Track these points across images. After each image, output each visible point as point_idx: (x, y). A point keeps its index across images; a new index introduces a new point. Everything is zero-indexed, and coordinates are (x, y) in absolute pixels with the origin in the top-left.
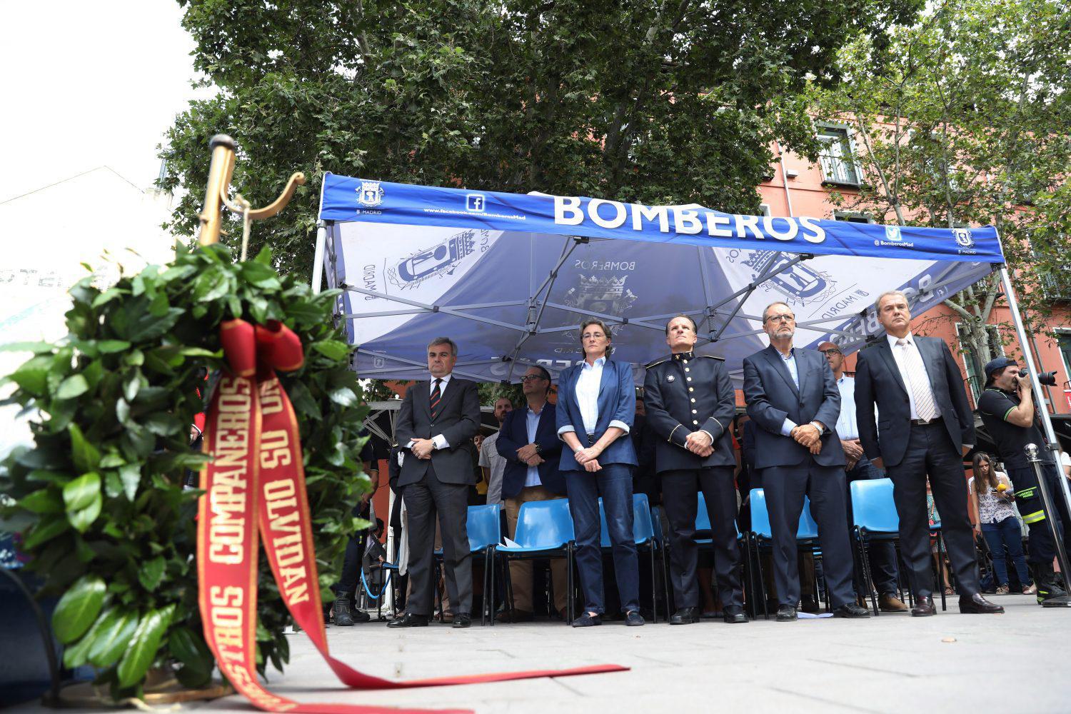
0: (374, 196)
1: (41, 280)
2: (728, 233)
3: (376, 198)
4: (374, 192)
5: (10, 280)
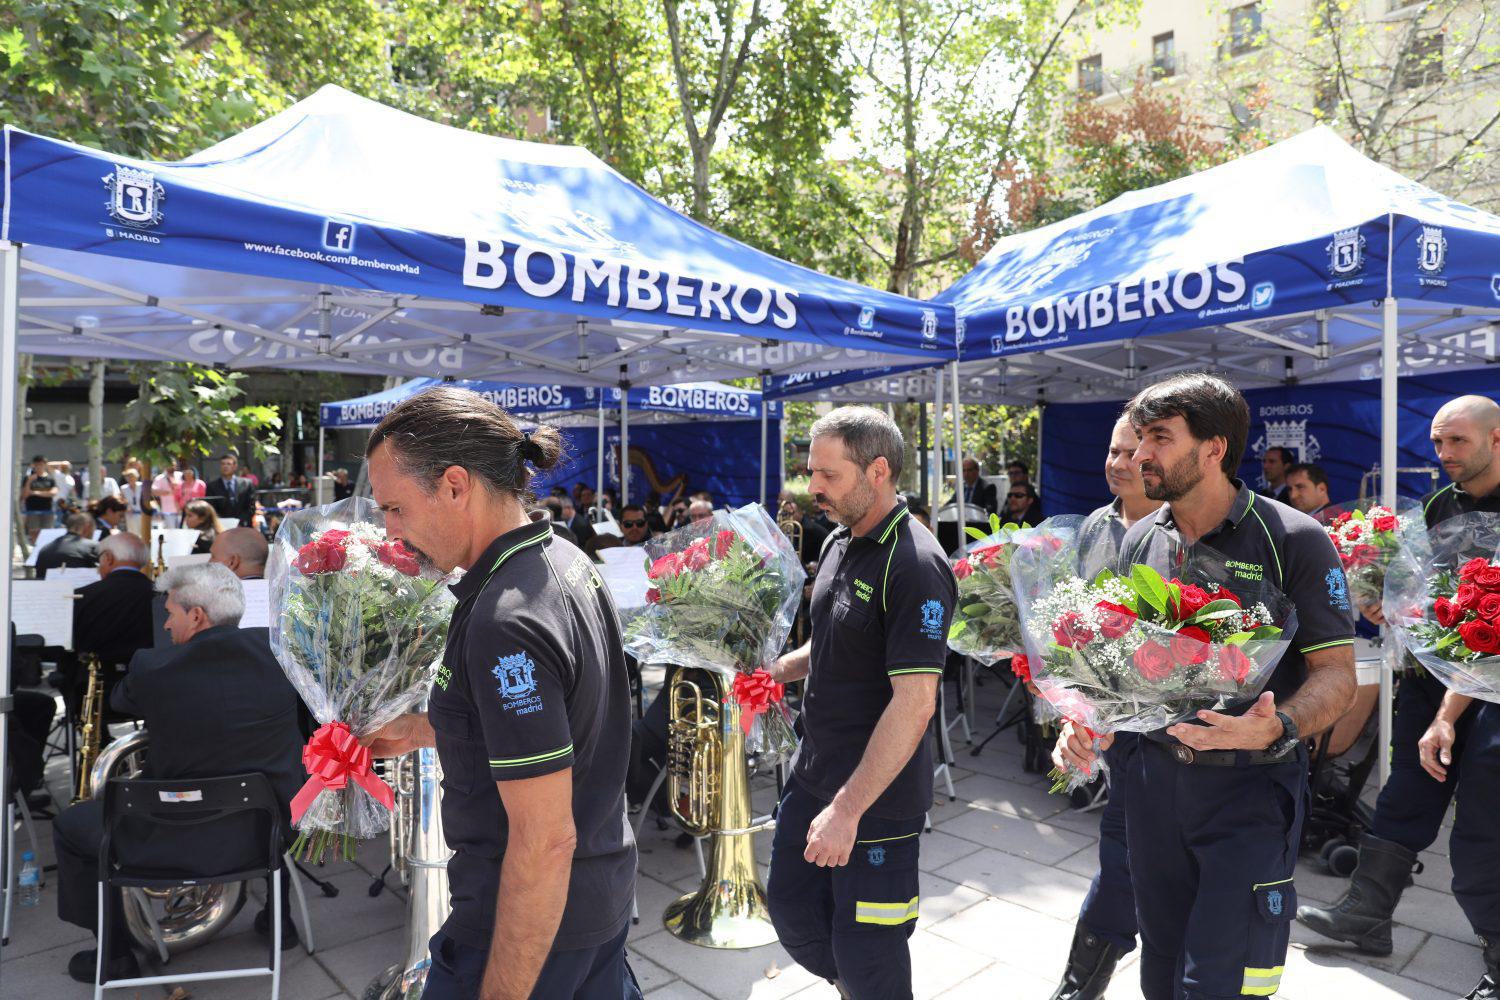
2: (690, 311)
4: (144, 191)
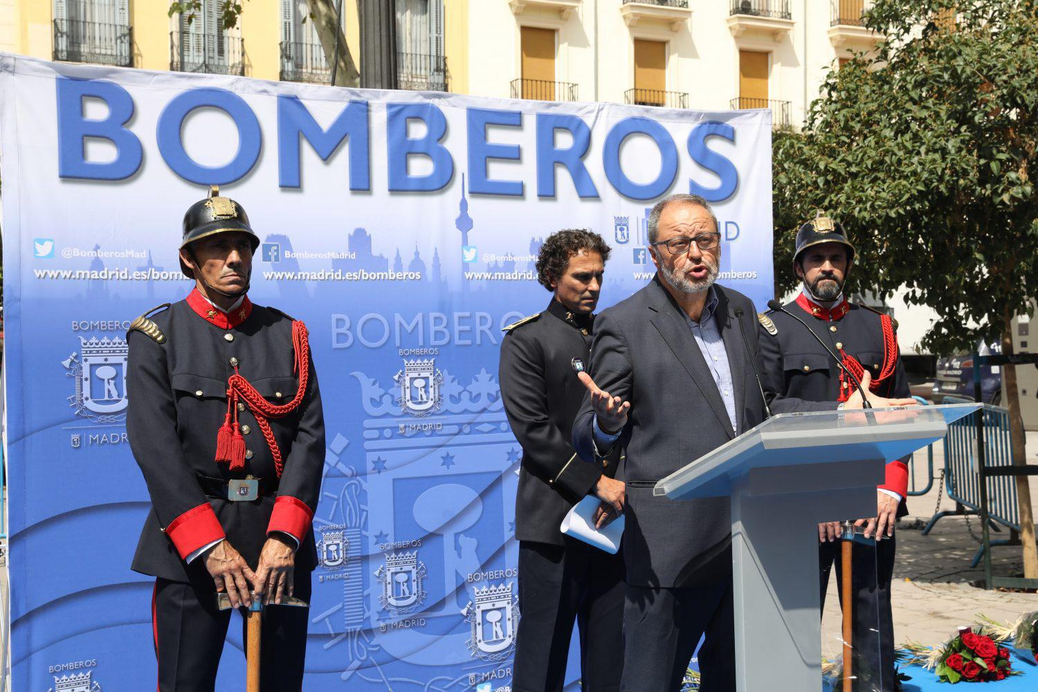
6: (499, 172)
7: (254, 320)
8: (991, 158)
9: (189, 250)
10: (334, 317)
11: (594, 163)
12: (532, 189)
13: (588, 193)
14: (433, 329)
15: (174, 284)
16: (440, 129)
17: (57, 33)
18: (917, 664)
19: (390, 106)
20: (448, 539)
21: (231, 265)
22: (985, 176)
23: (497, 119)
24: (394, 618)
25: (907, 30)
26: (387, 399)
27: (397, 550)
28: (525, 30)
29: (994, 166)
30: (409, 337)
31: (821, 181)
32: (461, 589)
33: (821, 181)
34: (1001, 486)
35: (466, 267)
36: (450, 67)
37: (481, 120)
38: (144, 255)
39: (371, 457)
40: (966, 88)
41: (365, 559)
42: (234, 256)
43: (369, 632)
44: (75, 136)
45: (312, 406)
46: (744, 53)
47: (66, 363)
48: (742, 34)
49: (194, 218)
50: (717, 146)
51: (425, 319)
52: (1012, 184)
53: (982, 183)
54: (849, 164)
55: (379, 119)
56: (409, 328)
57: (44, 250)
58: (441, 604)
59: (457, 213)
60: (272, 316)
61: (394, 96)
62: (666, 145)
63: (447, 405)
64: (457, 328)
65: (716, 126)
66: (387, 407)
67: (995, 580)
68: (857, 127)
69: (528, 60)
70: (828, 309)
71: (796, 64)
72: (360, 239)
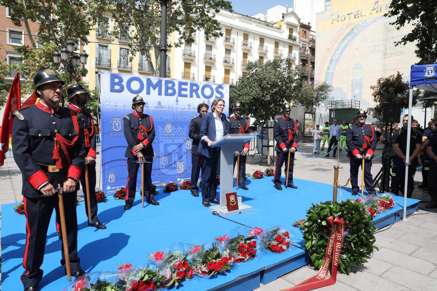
0: (432, 72)
1: (355, 16)
3: (433, 73)
4: (432, 71)
5: (344, 20)
6: (183, 92)
7: (144, 117)
8: (264, 93)
9: (134, 105)
10: (155, 116)
11: (199, 92)
12: (189, 95)
13: (198, 97)
14: (171, 119)
15: (132, 111)
16: (174, 85)
17: (96, 60)
18: (249, 176)
19: (165, 81)
20: (173, 154)
21: (141, 107)
22: (263, 96)
23: (183, 84)
24: (164, 167)
25: (253, 71)
26: (163, 130)
27: (164, 156)
28: (185, 63)
29: (264, 94)
30: (167, 120)
31: (237, 95)
32: (175, 162)
33: (237, 95)
34: (265, 149)
35: (177, 108)
36: (171, 69)
37: (181, 84)
38: (123, 105)
39: (160, 140)
40: (261, 80)
41: (159, 157)
42: (141, 106)
43: (160, 169)
44: (113, 84)
45: (153, 130)
46: (225, 70)
47: (111, 122)
48: (225, 66)
49: (134, 100)
50: (220, 90)
51: (170, 117)
52: (267, 97)
53: (263, 97)
54: (242, 93)
55: (163, 83)
56: (167, 118)
57: (107, 103)
58: (172, 165)
59: (176, 99)
60: (146, 116)
61: (167, 79)
62: (212, 89)
63: (173, 132)
64: (175, 119)
65: (220, 86)
66: (163, 132)
67: (263, 164)
68: (244, 87)
69: (185, 69)
70: (238, 118)
71: (235, 72)
72: (159, 103)
